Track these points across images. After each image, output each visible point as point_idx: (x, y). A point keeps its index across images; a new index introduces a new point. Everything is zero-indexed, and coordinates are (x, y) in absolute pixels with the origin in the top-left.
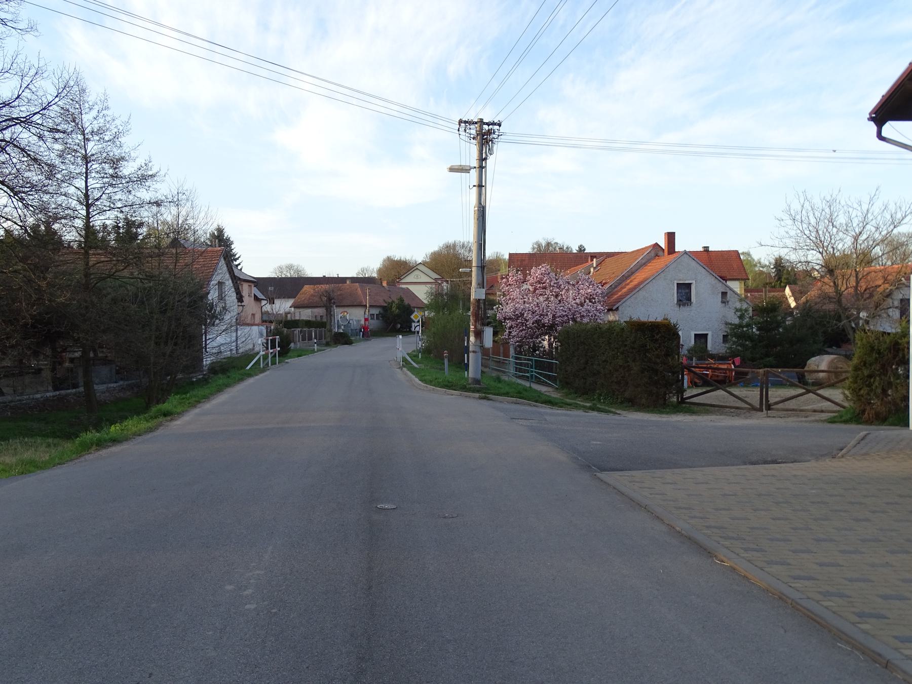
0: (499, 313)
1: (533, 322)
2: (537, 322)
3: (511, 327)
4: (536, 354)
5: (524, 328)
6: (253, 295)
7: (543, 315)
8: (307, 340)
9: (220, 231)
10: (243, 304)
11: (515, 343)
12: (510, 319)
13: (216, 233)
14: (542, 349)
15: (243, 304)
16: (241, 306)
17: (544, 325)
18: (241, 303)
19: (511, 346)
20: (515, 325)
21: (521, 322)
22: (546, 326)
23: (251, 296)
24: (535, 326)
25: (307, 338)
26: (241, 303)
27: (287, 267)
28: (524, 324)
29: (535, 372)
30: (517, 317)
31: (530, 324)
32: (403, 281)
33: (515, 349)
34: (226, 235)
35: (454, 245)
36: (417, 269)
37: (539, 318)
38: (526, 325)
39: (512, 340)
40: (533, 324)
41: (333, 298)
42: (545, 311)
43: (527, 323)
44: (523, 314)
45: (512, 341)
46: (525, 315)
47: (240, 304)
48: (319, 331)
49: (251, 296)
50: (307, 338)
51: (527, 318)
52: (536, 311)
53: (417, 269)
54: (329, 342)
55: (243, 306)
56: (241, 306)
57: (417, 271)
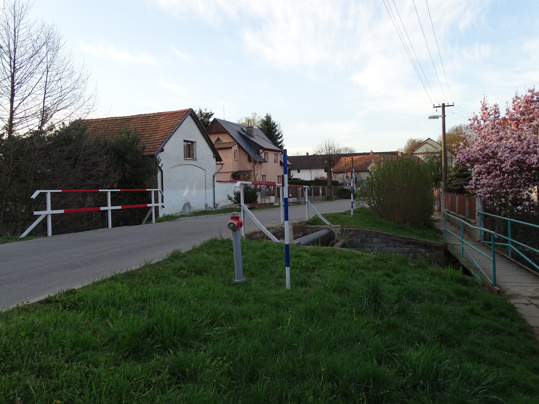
0: (460, 153)
1: (512, 163)
2: (519, 162)
3: (479, 173)
4: (517, 210)
5: (498, 172)
6: (279, 162)
7: (529, 153)
8: (313, 195)
9: (268, 118)
10: (222, 162)
11: (485, 194)
12: (476, 161)
13: (531, 199)
14: (527, 203)
15: (222, 162)
16: (221, 164)
17: (530, 169)
18: (220, 161)
19: (478, 200)
20: (485, 170)
21: (493, 165)
22: (532, 169)
23: (277, 162)
24: (515, 170)
25: (313, 193)
26: (220, 161)
27: (344, 149)
28: (498, 168)
29: (512, 243)
30: (487, 158)
31: (506, 166)
32: (415, 152)
33: (484, 203)
34: (272, 121)
35: (461, 127)
36: (426, 143)
37: (522, 158)
38: (501, 169)
39: (480, 190)
40: (511, 167)
41: (333, 161)
42: (531, 146)
43: (503, 165)
44: (497, 154)
45: (480, 192)
46: (500, 154)
47: (219, 162)
48: (334, 188)
49: (277, 162)
50: (313, 193)
51: (502, 158)
52: (516, 147)
53: (426, 143)
54: (330, 196)
55: (222, 164)
56: (221, 164)
57: (426, 144)
